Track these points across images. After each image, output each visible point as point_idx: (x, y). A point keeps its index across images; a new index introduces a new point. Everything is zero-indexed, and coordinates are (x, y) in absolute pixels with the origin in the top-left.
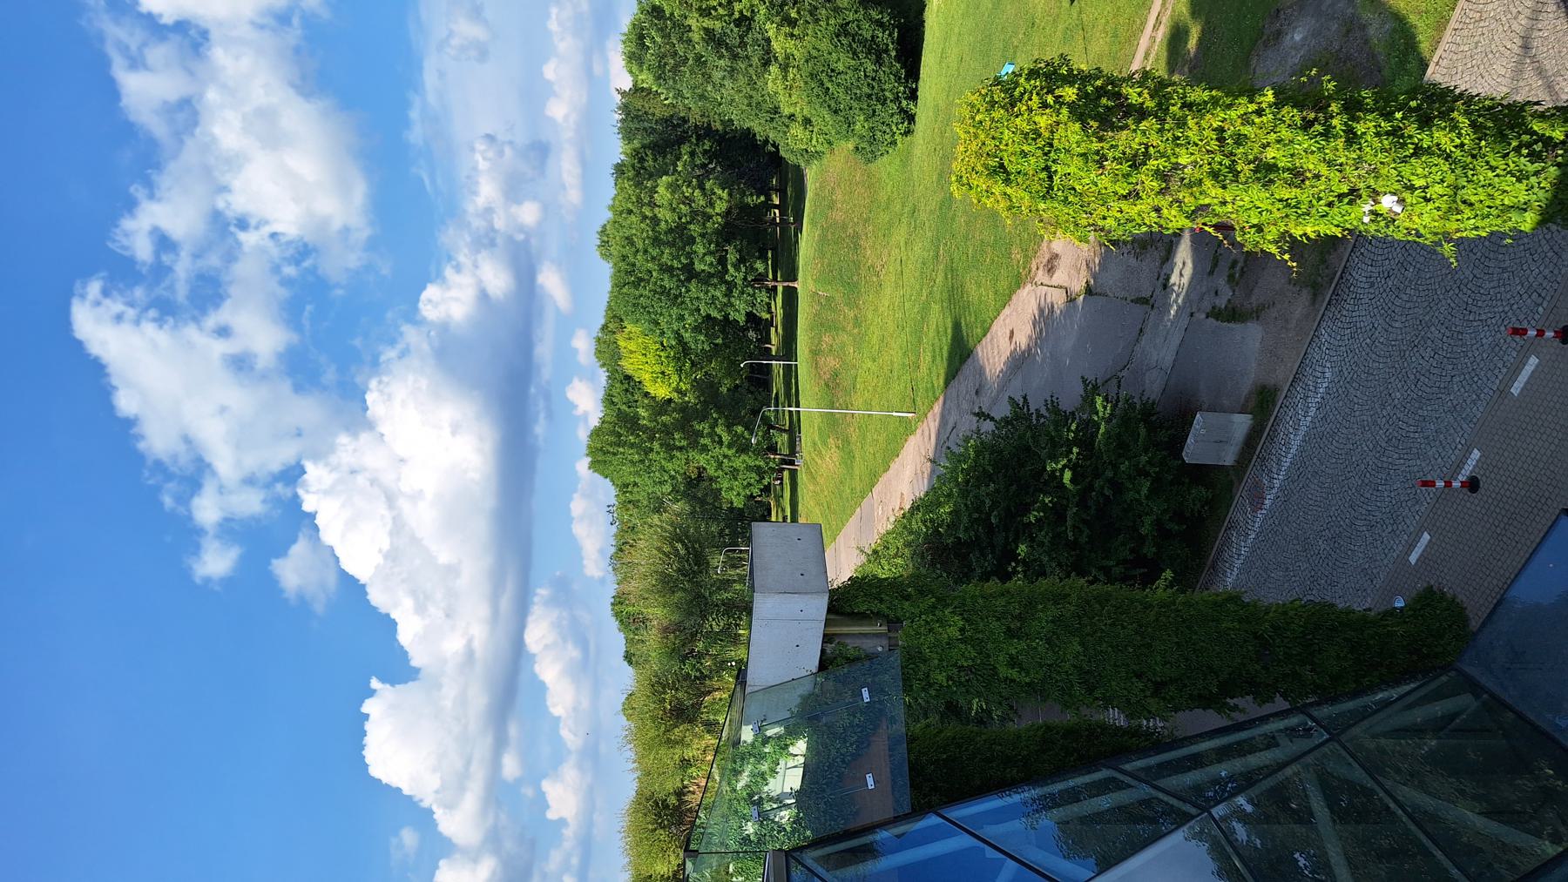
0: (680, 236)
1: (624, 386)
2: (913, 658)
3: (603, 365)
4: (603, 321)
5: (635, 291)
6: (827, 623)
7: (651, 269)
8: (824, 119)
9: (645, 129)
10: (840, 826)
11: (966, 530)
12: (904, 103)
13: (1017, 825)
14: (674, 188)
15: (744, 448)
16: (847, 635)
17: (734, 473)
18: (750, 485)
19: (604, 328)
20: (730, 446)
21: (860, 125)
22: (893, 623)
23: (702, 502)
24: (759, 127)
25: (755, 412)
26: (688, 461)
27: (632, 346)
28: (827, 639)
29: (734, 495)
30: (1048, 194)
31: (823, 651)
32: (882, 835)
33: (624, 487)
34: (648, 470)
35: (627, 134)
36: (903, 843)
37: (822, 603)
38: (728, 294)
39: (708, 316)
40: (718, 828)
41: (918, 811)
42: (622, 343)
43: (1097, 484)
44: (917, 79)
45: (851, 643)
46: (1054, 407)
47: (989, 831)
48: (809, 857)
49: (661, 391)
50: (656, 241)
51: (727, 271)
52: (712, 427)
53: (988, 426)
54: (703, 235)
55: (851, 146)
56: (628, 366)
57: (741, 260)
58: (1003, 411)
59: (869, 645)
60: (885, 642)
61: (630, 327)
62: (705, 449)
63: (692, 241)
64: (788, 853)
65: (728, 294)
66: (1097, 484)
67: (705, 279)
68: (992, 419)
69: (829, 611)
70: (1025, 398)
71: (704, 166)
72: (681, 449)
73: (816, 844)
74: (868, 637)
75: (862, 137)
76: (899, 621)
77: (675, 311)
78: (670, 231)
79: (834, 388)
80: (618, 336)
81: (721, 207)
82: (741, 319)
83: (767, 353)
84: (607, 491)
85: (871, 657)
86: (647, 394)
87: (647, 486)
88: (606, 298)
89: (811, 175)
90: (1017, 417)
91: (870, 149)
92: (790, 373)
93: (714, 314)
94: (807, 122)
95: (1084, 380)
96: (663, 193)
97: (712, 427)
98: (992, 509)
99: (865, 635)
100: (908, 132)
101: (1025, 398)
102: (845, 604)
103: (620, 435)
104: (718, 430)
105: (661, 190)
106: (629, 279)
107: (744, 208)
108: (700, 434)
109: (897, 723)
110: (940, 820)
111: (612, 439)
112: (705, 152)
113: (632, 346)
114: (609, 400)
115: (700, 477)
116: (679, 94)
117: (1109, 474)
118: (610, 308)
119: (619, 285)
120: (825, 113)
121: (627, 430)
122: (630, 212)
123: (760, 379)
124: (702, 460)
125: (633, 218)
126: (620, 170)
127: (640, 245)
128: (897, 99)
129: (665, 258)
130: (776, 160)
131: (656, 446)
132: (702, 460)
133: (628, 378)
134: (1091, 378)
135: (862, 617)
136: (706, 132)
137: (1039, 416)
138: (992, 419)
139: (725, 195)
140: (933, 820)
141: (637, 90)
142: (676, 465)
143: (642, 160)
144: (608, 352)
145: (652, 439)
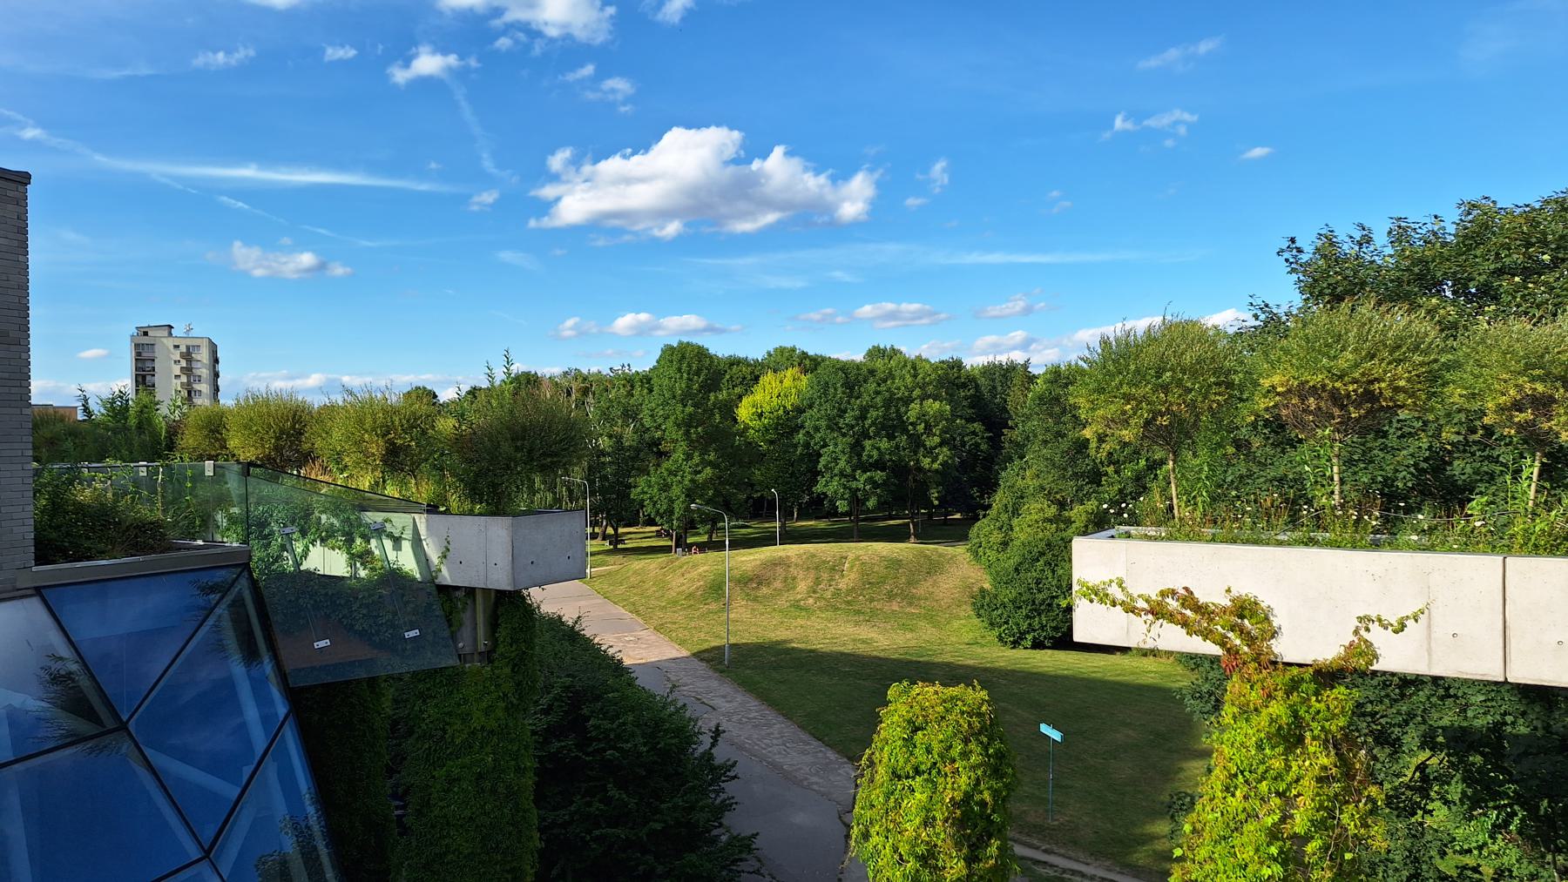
0: (893, 426)
1: (749, 374)
2: (451, 678)
3: (770, 355)
4: (811, 353)
5: (845, 382)
6: (486, 591)
7: (864, 394)
8: (1011, 559)
9: (994, 387)
10: (276, 619)
11: (597, 727)
12: (1029, 637)
13: (280, 808)
14: (940, 415)
15: (690, 495)
16: (474, 610)
17: (666, 487)
18: (655, 504)
19: (804, 355)
20: (692, 481)
21: (1008, 594)
22: (488, 656)
23: (634, 459)
24: (999, 499)
25: (727, 506)
26: (675, 441)
27: (787, 383)
28: (471, 591)
29: (643, 487)
30: (896, 775)
31: (457, 588)
32: (268, 667)
33: (646, 380)
34: (665, 403)
35: (990, 371)
36: (258, 687)
37: (505, 585)
38: (842, 474)
39: (820, 455)
40: (277, 494)
41: (294, 695)
42: (790, 372)
43: (650, 858)
44: (1054, 647)
45: (466, 617)
46: (726, 806)
47: (271, 770)
48: (244, 582)
49: (744, 412)
50: (888, 403)
51: (864, 472)
52: (710, 463)
53: (707, 740)
54: (897, 447)
55: (987, 586)
56: (768, 379)
57: (875, 485)
58: (721, 754)
59: (466, 633)
60: (468, 650)
61: (805, 380)
62: (689, 457)
63: (891, 437)
64: (246, 567)
65: (842, 474)
66: (650, 858)
67: (856, 448)
68: (713, 745)
69: (498, 592)
70: (735, 777)
71: (963, 444)
72: (687, 433)
73: (254, 584)
74: (474, 633)
75: (996, 596)
76: (491, 661)
77: (823, 423)
78: (900, 417)
79: (752, 582)
80: (797, 369)
81: (926, 462)
82: (819, 488)
83: (786, 515)
84: (644, 362)
85: (454, 637)
86: (740, 397)
87: (649, 406)
88: (834, 356)
89: (960, 551)
90: (713, 769)
91: (983, 604)
92: (767, 540)
93: (823, 461)
94: (1005, 544)
95: (755, 835)
96: (933, 406)
97: (710, 463)
98: (620, 750)
99: (475, 628)
100: (1000, 638)
101: (735, 777)
102: (508, 606)
103: (698, 373)
104: (708, 470)
105: (937, 405)
106: (851, 377)
107: (923, 487)
108: (704, 452)
109: (389, 665)
110: (281, 717)
111: (694, 367)
112: (977, 445)
113: (787, 383)
114: (734, 362)
115: (660, 454)
116: (1028, 418)
117: (660, 869)
118: (824, 359)
119: (844, 368)
120: (1017, 559)
121: (703, 378)
122: (915, 376)
123: (760, 509)
124: (679, 455)
125: (909, 379)
126: (957, 365)
127: (883, 388)
128: (1031, 629)
129: (873, 414)
130: (974, 511)
131: (689, 409)
132: (679, 455)
133: (757, 379)
134: (758, 843)
135: (493, 625)
136: (995, 442)
137: (717, 793)
138: (713, 745)
139: (935, 466)
140: (282, 710)
141: (1032, 379)
142: (672, 432)
143: (964, 386)
144: (785, 359)
145: (695, 406)
